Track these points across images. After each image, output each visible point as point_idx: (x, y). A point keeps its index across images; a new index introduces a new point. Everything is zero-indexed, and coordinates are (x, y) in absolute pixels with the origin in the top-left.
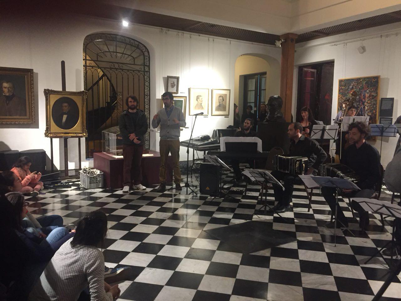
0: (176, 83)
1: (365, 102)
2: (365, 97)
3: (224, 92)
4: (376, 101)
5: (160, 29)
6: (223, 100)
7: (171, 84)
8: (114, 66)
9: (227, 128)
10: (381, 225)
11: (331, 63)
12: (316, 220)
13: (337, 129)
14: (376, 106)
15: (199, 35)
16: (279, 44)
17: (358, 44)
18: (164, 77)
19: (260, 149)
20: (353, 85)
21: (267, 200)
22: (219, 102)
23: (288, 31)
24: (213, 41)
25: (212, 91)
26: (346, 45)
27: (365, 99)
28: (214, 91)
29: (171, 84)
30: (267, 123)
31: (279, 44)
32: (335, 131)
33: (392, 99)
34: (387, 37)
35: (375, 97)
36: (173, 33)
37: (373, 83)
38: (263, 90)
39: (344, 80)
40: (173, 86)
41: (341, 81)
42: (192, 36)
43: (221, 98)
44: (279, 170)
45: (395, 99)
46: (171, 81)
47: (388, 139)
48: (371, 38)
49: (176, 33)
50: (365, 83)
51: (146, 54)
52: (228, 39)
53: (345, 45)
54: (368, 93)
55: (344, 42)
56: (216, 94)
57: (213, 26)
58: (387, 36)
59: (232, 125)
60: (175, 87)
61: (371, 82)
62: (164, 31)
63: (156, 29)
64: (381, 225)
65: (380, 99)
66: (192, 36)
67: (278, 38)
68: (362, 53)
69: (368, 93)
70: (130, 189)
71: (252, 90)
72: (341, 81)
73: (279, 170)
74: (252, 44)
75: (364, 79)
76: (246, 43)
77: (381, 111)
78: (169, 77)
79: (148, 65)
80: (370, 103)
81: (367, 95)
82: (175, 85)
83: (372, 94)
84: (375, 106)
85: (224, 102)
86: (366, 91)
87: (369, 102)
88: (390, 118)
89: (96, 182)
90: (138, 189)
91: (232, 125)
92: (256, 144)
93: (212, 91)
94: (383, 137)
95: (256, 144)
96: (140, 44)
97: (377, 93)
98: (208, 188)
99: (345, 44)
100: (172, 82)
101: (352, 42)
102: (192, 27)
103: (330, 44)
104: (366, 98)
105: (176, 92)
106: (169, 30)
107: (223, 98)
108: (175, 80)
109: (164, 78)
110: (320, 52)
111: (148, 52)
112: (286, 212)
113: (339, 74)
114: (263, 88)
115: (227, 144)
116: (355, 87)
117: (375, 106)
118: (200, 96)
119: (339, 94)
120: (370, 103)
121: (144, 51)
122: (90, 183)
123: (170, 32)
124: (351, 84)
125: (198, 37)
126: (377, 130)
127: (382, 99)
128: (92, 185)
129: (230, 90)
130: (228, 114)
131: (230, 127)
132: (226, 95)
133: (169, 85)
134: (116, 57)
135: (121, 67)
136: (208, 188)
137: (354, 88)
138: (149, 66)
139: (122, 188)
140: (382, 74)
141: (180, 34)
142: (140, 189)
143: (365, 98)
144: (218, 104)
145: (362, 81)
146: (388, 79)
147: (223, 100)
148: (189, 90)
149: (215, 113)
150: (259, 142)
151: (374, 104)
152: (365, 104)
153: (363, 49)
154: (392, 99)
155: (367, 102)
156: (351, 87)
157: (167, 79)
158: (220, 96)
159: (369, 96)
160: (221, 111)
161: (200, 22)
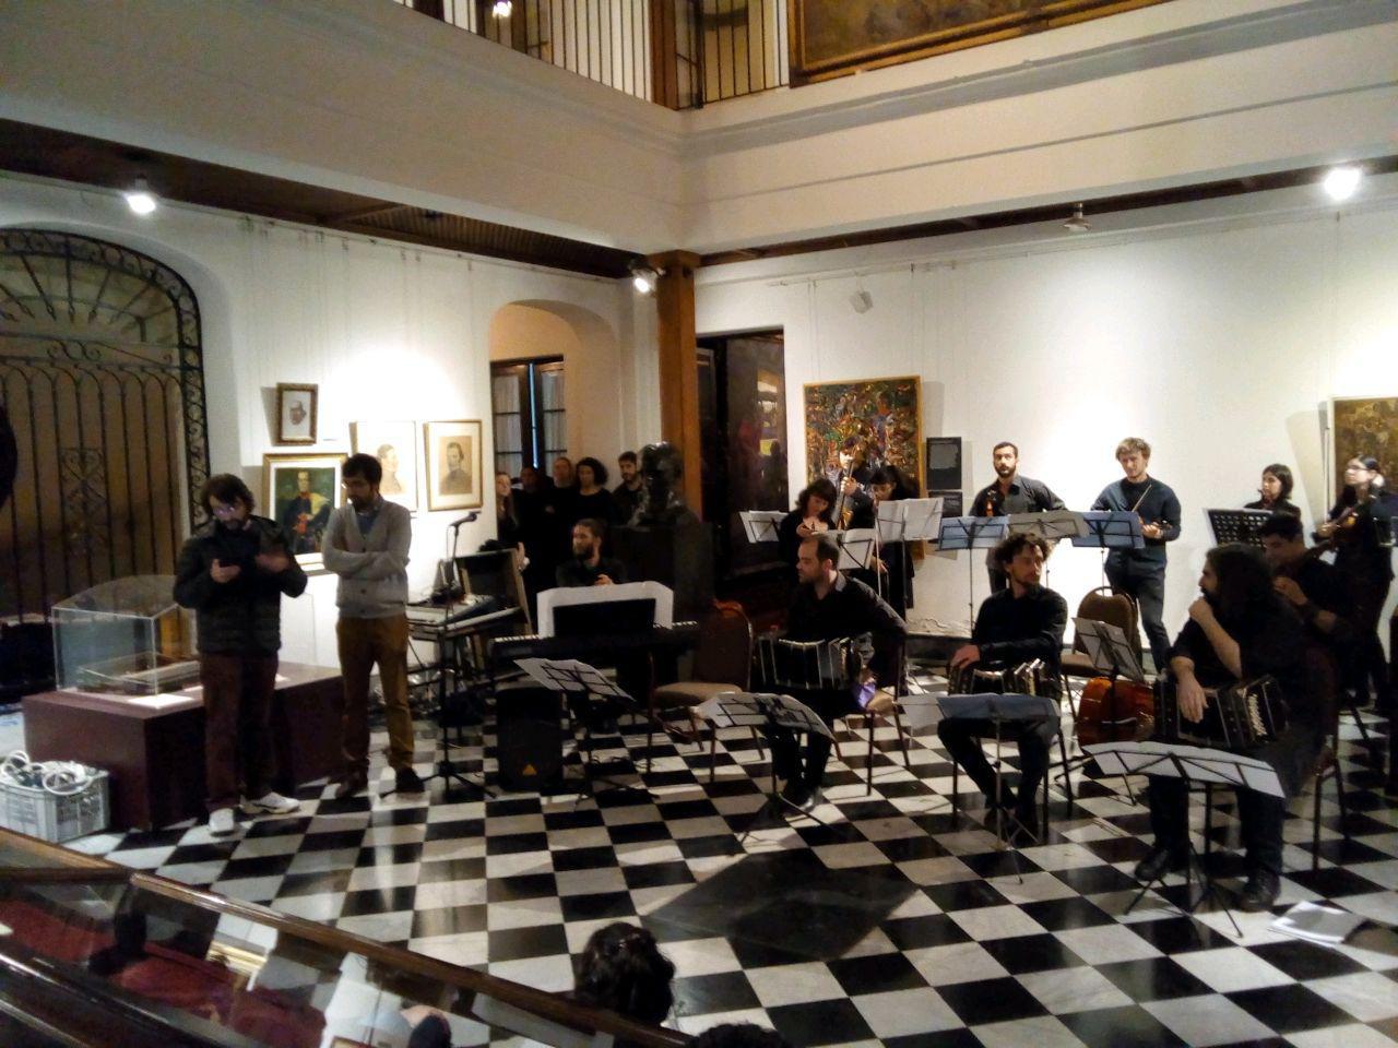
0: (307, 408)
1: (884, 448)
2: (884, 433)
3: (459, 431)
4: (914, 446)
5: (241, 218)
6: (462, 456)
7: (293, 410)
8: (65, 350)
9: (483, 548)
10: (1064, 799)
11: (772, 337)
12: (911, 818)
13: (870, 540)
14: (916, 462)
15: (373, 241)
16: (643, 284)
17: (851, 285)
18: (266, 386)
19: (664, 617)
20: (847, 402)
21: (716, 780)
22: (450, 465)
23: (675, 246)
24: (418, 259)
25: (426, 429)
26: (815, 285)
27: (883, 441)
28: (432, 428)
29: (293, 410)
30: (645, 529)
31: (643, 284)
32: (867, 544)
33: (957, 442)
34: (929, 270)
35: (912, 434)
36: (333, 238)
37: (903, 395)
38: (548, 411)
39: (821, 387)
40: (297, 419)
41: (810, 391)
42: (350, 244)
43: (455, 451)
44: (777, 682)
45: (963, 440)
46: (291, 400)
47: (956, 555)
48: (884, 272)
49: (294, 234)
50: (882, 396)
51: (185, 304)
52: (461, 253)
53: (812, 286)
54: (890, 424)
55: (808, 279)
56: (442, 434)
57: (432, 216)
58: (928, 267)
59: (494, 536)
60: (306, 422)
61: (897, 393)
62: (257, 226)
63: (230, 220)
64: (1064, 799)
65: (925, 441)
66: (423, 256)
67: (642, 263)
68: (862, 312)
69: (890, 424)
70: (240, 816)
71: (509, 411)
72: (810, 391)
73: (777, 682)
74: (533, 269)
75: (878, 384)
76: (486, 262)
77: (930, 473)
78: (282, 389)
79: (195, 343)
80: (897, 453)
81: (889, 430)
82: (304, 414)
83: (902, 427)
84: (912, 462)
85: (463, 463)
86: (883, 419)
87: (895, 449)
88: (957, 494)
89: (83, 813)
90: (266, 813)
91: (494, 536)
92: (649, 606)
93: (426, 429)
94: (974, 551)
95: (649, 606)
96: (161, 270)
97: (915, 425)
98: (530, 770)
99: (812, 283)
100: (295, 405)
101: (836, 276)
102: (363, 216)
103: (764, 282)
104: (887, 438)
105: (308, 437)
106: (272, 223)
107: (459, 449)
108: (305, 398)
109: (266, 391)
110: (730, 304)
111: (192, 296)
112: (984, 831)
113: (807, 365)
114: (548, 405)
115: (561, 613)
116: (854, 407)
117: (912, 462)
118: (390, 447)
119: (808, 426)
120: (897, 453)
121: (175, 293)
122: (60, 820)
123: (273, 230)
124: (839, 400)
125: (369, 245)
126: (961, 531)
127: (929, 441)
128: (68, 826)
129: (479, 422)
130: (477, 501)
131: (489, 545)
132: (469, 438)
133: (287, 413)
134: (55, 318)
135: (92, 353)
136: (530, 770)
137: (850, 408)
138: (199, 351)
139: (203, 820)
140: (926, 373)
141: (411, 255)
142: (276, 811)
143: (884, 439)
144: (447, 471)
145: (873, 389)
146: (941, 387)
147: (462, 456)
148: (353, 429)
149: (441, 500)
150: (664, 597)
151: (910, 456)
152: (885, 454)
153: (865, 301)
154: (957, 442)
155: (891, 450)
156: (840, 407)
157: (275, 394)
158: (451, 445)
159: (896, 432)
160: (456, 492)
161: (393, 205)
